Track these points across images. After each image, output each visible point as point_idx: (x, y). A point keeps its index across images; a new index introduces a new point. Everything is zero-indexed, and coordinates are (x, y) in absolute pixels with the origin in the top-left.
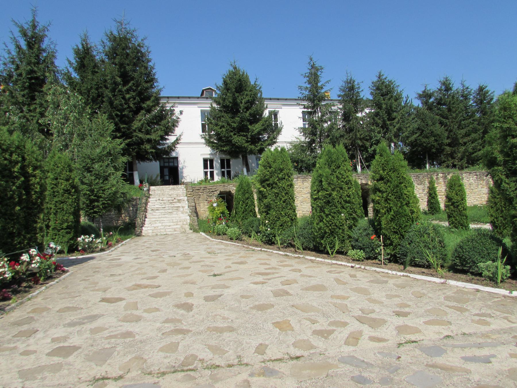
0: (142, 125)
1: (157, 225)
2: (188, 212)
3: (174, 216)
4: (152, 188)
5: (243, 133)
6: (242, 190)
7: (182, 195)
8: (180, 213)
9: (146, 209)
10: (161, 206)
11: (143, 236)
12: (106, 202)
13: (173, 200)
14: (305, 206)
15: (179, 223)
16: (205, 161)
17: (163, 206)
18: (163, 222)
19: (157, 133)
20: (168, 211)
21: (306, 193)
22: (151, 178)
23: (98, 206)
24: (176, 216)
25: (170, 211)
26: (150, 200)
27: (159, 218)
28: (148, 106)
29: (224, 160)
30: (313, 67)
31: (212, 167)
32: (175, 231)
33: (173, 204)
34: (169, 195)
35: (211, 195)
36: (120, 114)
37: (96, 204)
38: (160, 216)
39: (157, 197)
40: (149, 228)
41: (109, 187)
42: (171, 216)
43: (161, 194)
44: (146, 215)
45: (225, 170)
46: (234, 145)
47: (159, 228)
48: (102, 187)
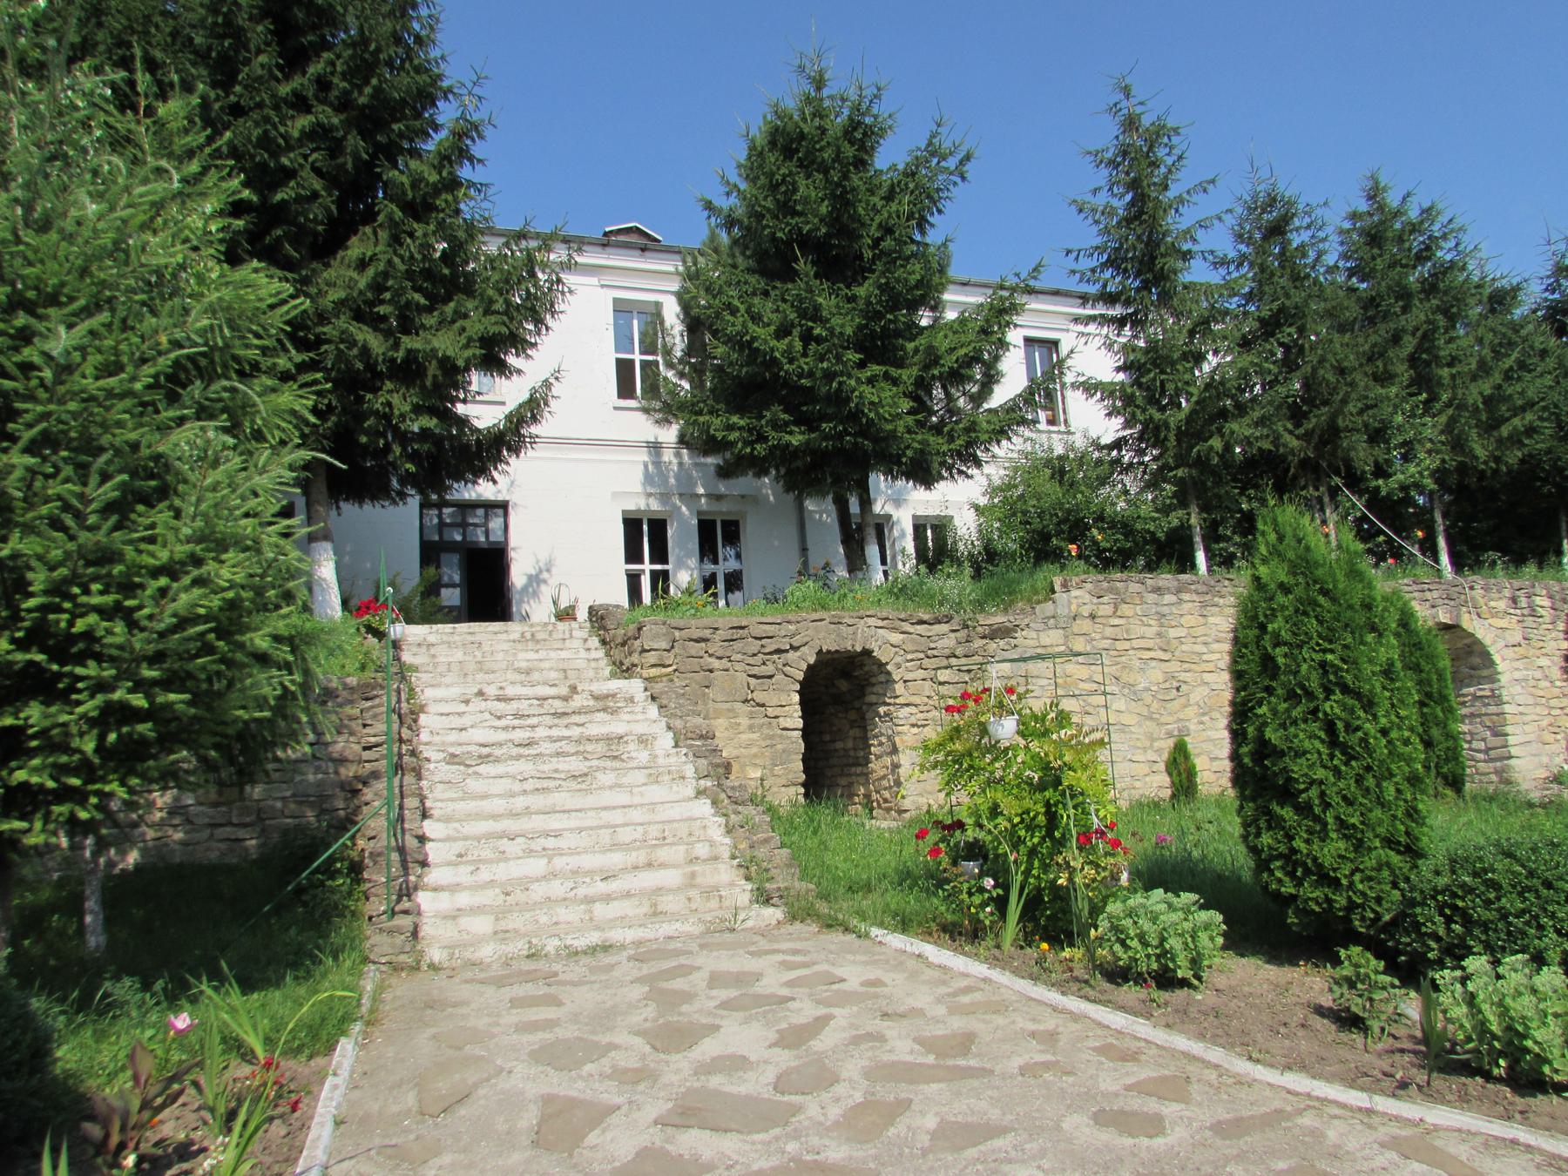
0: (378, 287)
1: (515, 870)
2: (689, 771)
3: (609, 798)
7: (591, 674)
11: (433, 967)
12: (139, 701)
15: (663, 854)
16: (632, 525)
17: (519, 735)
18: (551, 843)
20: (556, 763)
23: (54, 742)
24: (622, 798)
25: (575, 765)
27: (514, 815)
29: (714, 522)
31: (660, 554)
32: (656, 914)
34: (519, 671)
35: (769, 669)
37: (34, 714)
38: (520, 802)
41: (181, 550)
42: (591, 801)
43: (471, 667)
47: (539, 891)
48: (107, 557)
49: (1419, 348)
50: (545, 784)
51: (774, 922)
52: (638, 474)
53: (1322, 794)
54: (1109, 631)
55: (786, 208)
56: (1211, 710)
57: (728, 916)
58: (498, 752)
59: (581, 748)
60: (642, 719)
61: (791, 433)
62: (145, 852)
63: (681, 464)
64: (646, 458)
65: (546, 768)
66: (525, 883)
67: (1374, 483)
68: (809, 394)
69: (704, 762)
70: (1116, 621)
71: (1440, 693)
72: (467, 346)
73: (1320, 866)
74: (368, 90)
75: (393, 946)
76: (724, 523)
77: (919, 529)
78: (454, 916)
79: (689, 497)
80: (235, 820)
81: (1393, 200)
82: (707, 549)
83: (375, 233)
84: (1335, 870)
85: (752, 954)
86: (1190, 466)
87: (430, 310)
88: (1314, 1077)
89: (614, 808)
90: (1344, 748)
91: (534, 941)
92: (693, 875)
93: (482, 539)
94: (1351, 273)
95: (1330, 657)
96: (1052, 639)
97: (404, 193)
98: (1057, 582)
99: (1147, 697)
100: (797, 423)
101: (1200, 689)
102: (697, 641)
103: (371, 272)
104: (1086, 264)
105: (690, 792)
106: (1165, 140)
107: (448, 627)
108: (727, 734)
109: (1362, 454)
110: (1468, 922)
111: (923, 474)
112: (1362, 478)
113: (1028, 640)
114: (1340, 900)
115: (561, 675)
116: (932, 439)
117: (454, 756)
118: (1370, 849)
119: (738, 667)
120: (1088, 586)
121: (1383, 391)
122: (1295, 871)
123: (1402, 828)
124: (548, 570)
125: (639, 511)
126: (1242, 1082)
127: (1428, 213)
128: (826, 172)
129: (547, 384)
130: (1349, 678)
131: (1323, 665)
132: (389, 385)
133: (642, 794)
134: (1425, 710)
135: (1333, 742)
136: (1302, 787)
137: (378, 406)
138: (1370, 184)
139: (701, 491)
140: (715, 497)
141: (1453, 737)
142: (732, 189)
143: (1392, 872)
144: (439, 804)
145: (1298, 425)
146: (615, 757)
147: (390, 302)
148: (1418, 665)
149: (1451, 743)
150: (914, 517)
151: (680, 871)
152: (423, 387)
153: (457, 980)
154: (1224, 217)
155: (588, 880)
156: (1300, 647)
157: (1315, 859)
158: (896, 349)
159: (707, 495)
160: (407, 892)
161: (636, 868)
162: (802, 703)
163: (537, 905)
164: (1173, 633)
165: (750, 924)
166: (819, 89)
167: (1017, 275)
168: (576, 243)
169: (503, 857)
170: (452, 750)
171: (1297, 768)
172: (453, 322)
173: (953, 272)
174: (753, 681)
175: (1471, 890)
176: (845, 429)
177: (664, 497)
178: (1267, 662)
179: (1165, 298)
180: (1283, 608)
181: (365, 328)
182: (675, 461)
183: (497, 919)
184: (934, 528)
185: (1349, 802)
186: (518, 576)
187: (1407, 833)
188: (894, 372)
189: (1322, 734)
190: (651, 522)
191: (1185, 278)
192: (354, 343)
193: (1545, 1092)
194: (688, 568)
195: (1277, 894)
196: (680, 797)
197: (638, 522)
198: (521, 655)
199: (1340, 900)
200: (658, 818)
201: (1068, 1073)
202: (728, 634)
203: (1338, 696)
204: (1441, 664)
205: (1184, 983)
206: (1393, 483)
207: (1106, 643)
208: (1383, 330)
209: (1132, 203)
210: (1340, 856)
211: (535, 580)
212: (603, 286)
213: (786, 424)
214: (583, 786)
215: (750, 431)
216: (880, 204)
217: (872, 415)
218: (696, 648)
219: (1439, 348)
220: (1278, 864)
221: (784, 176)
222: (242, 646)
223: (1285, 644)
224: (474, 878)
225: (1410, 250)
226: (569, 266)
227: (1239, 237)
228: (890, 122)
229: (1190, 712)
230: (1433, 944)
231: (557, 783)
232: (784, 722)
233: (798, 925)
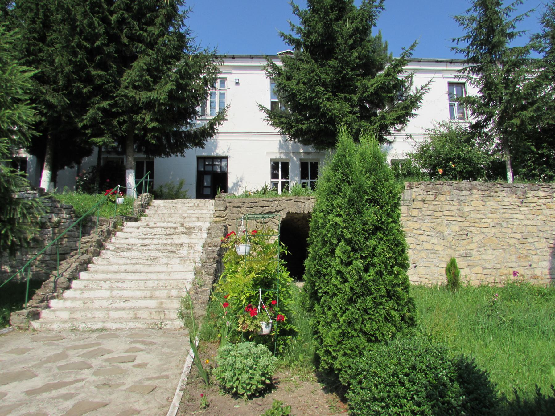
2: (198, 260)
5: (343, 95)
6: (348, 189)
8: (177, 260)
11: (34, 330)
14: (491, 257)
15: (158, 293)
16: (275, 165)
17: (147, 242)
21: (492, 224)
29: (307, 163)
31: (285, 175)
35: (266, 220)
42: (151, 269)
46: (324, 115)
47: (97, 303)
50: (140, 261)
52: (277, 145)
54: (431, 207)
56: (485, 245)
58: (134, 248)
59: (166, 248)
70: (436, 203)
75: (19, 320)
76: (311, 163)
79: (297, 153)
82: (304, 175)
91: (75, 324)
99: (450, 238)
101: (479, 235)
102: (236, 207)
104: (464, 45)
120: (422, 187)
124: (241, 181)
125: (277, 159)
132: (144, 111)
133: (172, 268)
139: (302, 151)
140: (306, 153)
142: (299, 31)
146: (174, 252)
154: (528, 14)
155: (118, 301)
156: (329, 213)
159: (304, 153)
161: (146, 298)
163: (96, 309)
164: (466, 209)
167: (403, 49)
168: (222, 58)
170: (117, 246)
174: (258, 224)
177: (287, 153)
186: (230, 184)
188: (348, 96)
190: (282, 163)
196: (187, 270)
197: (306, 164)
200: (171, 278)
207: (429, 213)
211: (236, 185)
213: (302, 120)
218: (235, 210)
224: (81, 296)
229: (473, 246)
231: (144, 261)
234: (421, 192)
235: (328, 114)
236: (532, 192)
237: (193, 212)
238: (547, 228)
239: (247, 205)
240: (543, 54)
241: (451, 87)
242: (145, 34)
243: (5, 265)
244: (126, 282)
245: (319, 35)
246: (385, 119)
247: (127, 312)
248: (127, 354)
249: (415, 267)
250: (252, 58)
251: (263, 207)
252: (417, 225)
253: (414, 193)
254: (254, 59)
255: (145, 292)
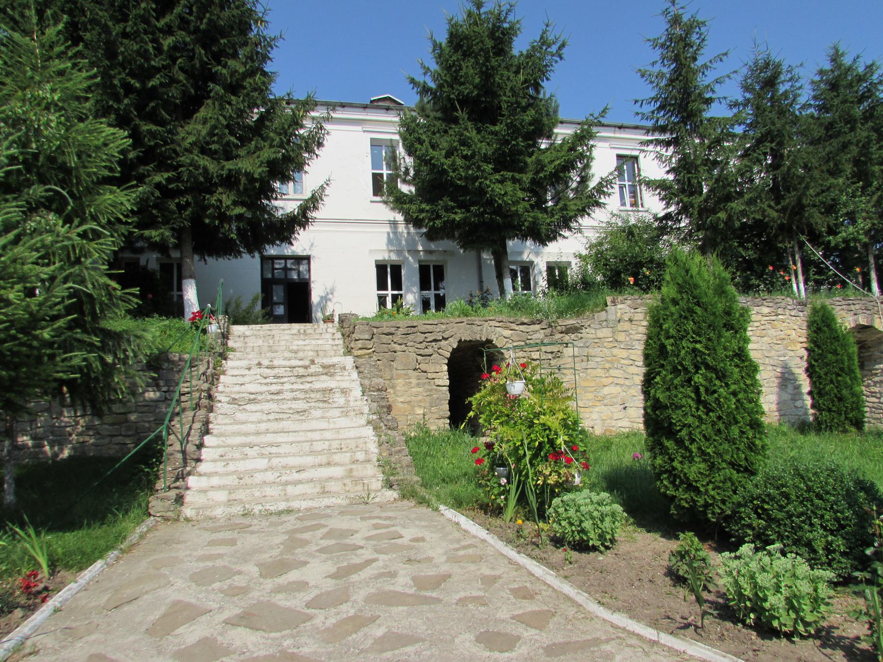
2: (366, 410)
3: (315, 425)
4: (238, 330)
7: (333, 353)
9: (210, 397)
10: (265, 388)
11: (187, 520)
13: (306, 367)
15: (337, 458)
16: (381, 268)
17: (274, 388)
18: (274, 450)
19: (258, 157)
22: (238, 306)
24: (323, 425)
25: (300, 405)
26: (228, 364)
27: (258, 433)
28: (234, 73)
29: (429, 266)
30: (676, 21)
31: (397, 285)
32: (324, 493)
33: (309, 379)
34: (291, 351)
35: (429, 351)
36: (138, 85)
39: (250, 356)
40: (215, 481)
42: (305, 426)
43: (265, 349)
44: (207, 423)
45: (431, 294)
47: (259, 478)
49: (861, 154)
50: (281, 416)
51: (392, 499)
53: (690, 433)
55: (456, 80)
57: (364, 495)
58: (260, 397)
59: (308, 396)
60: (351, 380)
61: (456, 213)
62: (74, 448)
63: (408, 233)
64: (389, 230)
65: (284, 407)
66: (251, 473)
67: (827, 239)
68: (464, 190)
69: (375, 404)
71: (849, 367)
72: (260, 166)
73: (688, 479)
74: (205, 21)
75: (164, 507)
76: (434, 266)
77: (550, 269)
78: (204, 491)
79: (414, 252)
80: (123, 433)
81: (847, 61)
82: (424, 285)
83: (214, 104)
84: (696, 482)
85: (362, 519)
86: (706, 230)
87: (243, 146)
88: (630, 618)
89: (316, 430)
90: (705, 404)
91: (247, 506)
92: (351, 470)
93: (295, 277)
94: (820, 108)
95: (698, 346)
96: (604, 333)
97: (226, 80)
98: (609, 299)
100: (460, 207)
102: (386, 334)
103: (208, 126)
104: (648, 109)
105: (363, 421)
106: (697, 30)
107: (258, 327)
108: (403, 388)
109: (820, 221)
110: (770, 519)
111: (543, 237)
112: (820, 235)
113: (588, 333)
114: (701, 501)
115: (315, 354)
116: (540, 215)
117: (234, 399)
118: (719, 469)
119: (411, 349)
120: (629, 302)
121: (835, 182)
122: (675, 481)
123: (743, 456)
124: (332, 294)
125: (384, 260)
126: (590, 617)
127: (870, 68)
128: (476, 57)
129: (322, 188)
130: (709, 359)
131: (694, 350)
132: (220, 190)
134: (839, 378)
135: (699, 401)
136: (678, 428)
137: (213, 202)
138: (832, 52)
139: (420, 248)
140: (428, 252)
141: (857, 396)
143: (733, 484)
144: (217, 427)
145: (777, 203)
146: (325, 401)
147: (217, 143)
148: (836, 350)
149: (855, 399)
150: (548, 263)
151: (343, 468)
152: (238, 190)
153: (195, 528)
154: (732, 76)
155: (288, 472)
156: (681, 339)
157: (685, 474)
158: (519, 161)
160: (181, 477)
162: (449, 371)
165: (377, 500)
166: (478, 8)
169: (245, 457)
170: (233, 396)
171: (676, 416)
172: (254, 152)
173: (561, 116)
174: (419, 358)
175: (772, 498)
176: (485, 210)
177: (399, 252)
178: (663, 347)
179: (695, 130)
180: (672, 314)
181: (206, 157)
182: (405, 231)
183: (230, 493)
184: (560, 269)
185: (707, 439)
186: (315, 298)
187: (746, 459)
188: (517, 176)
189: (693, 395)
190: (392, 267)
191: (707, 115)
192: (197, 167)
193: (778, 637)
194: (412, 292)
195: (665, 494)
196: (357, 425)
198: (296, 343)
199: (701, 501)
200: (341, 437)
201: (483, 605)
202: (405, 331)
203: (703, 371)
204: (850, 351)
205: (594, 549)
206: (839, 238)
208: (836, 143)
209: (675, 71)
210: (700, 473)
211: (325, 299)
212: (364, 131)
213: (453, 208)
214: (303, 418)
215: (432, 212)
216: (512, 75)
217: (500, 202)
218: (386, 339)
219: (872, 154)
220: (665, 476)
221: (454, 61)
222: (36, 338)
223: (673, 337)
224: (225, 469)
225: (857, 92)
226: (328, 119)
227: (746, 88)
228: (518, 26)
230: (750, 532)
232: (438, 382)
233: (405, 502)
234: (628, 309)
235: (496, 201)
236: (755, 308)
237: (304, 343)
238: (773, 353)
239: (402, 330)
240: (743, 127)
241: (621, 162)
242: (224, 71)
243: (23, 435)
244: (283, 445)
245: (475, 87)
246: (567, 210)
247: (312, 485)
248: (201, 565)
249: (625, 408)
250: (344, 107)
251: (425, 333)
252: (624, 354)
253: (619, 311)
254: (345, 109)
255: (320, 457)
